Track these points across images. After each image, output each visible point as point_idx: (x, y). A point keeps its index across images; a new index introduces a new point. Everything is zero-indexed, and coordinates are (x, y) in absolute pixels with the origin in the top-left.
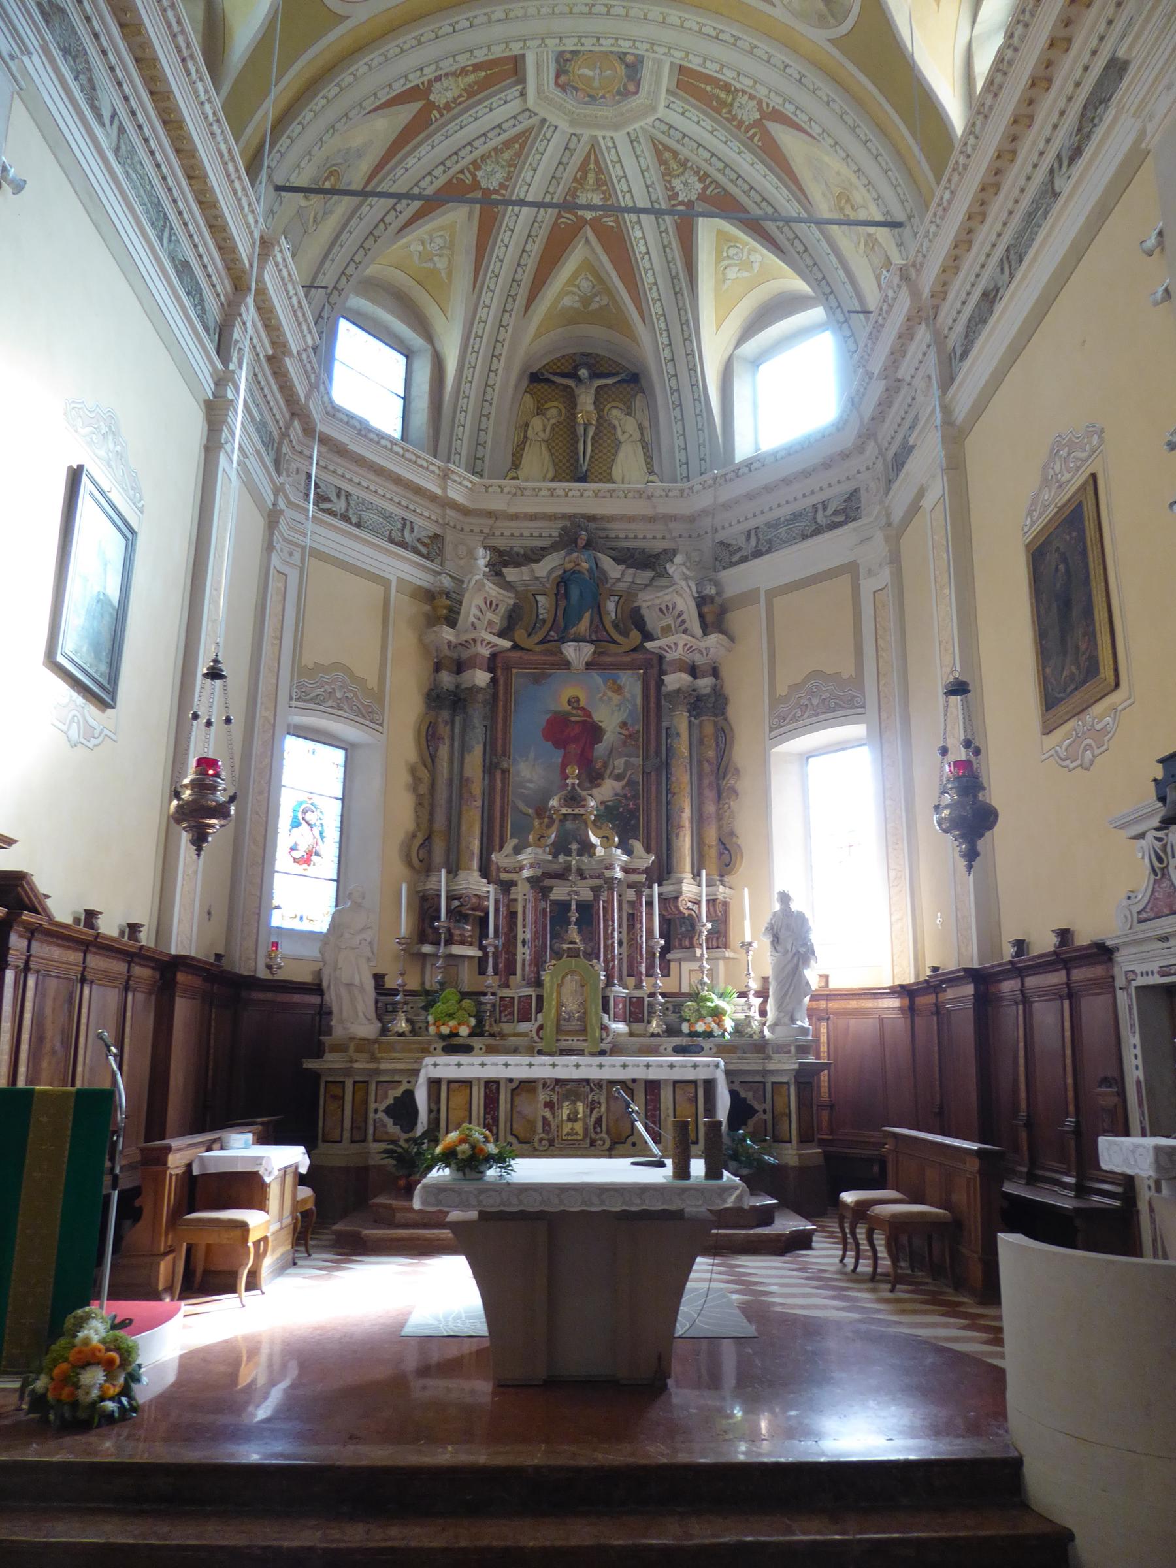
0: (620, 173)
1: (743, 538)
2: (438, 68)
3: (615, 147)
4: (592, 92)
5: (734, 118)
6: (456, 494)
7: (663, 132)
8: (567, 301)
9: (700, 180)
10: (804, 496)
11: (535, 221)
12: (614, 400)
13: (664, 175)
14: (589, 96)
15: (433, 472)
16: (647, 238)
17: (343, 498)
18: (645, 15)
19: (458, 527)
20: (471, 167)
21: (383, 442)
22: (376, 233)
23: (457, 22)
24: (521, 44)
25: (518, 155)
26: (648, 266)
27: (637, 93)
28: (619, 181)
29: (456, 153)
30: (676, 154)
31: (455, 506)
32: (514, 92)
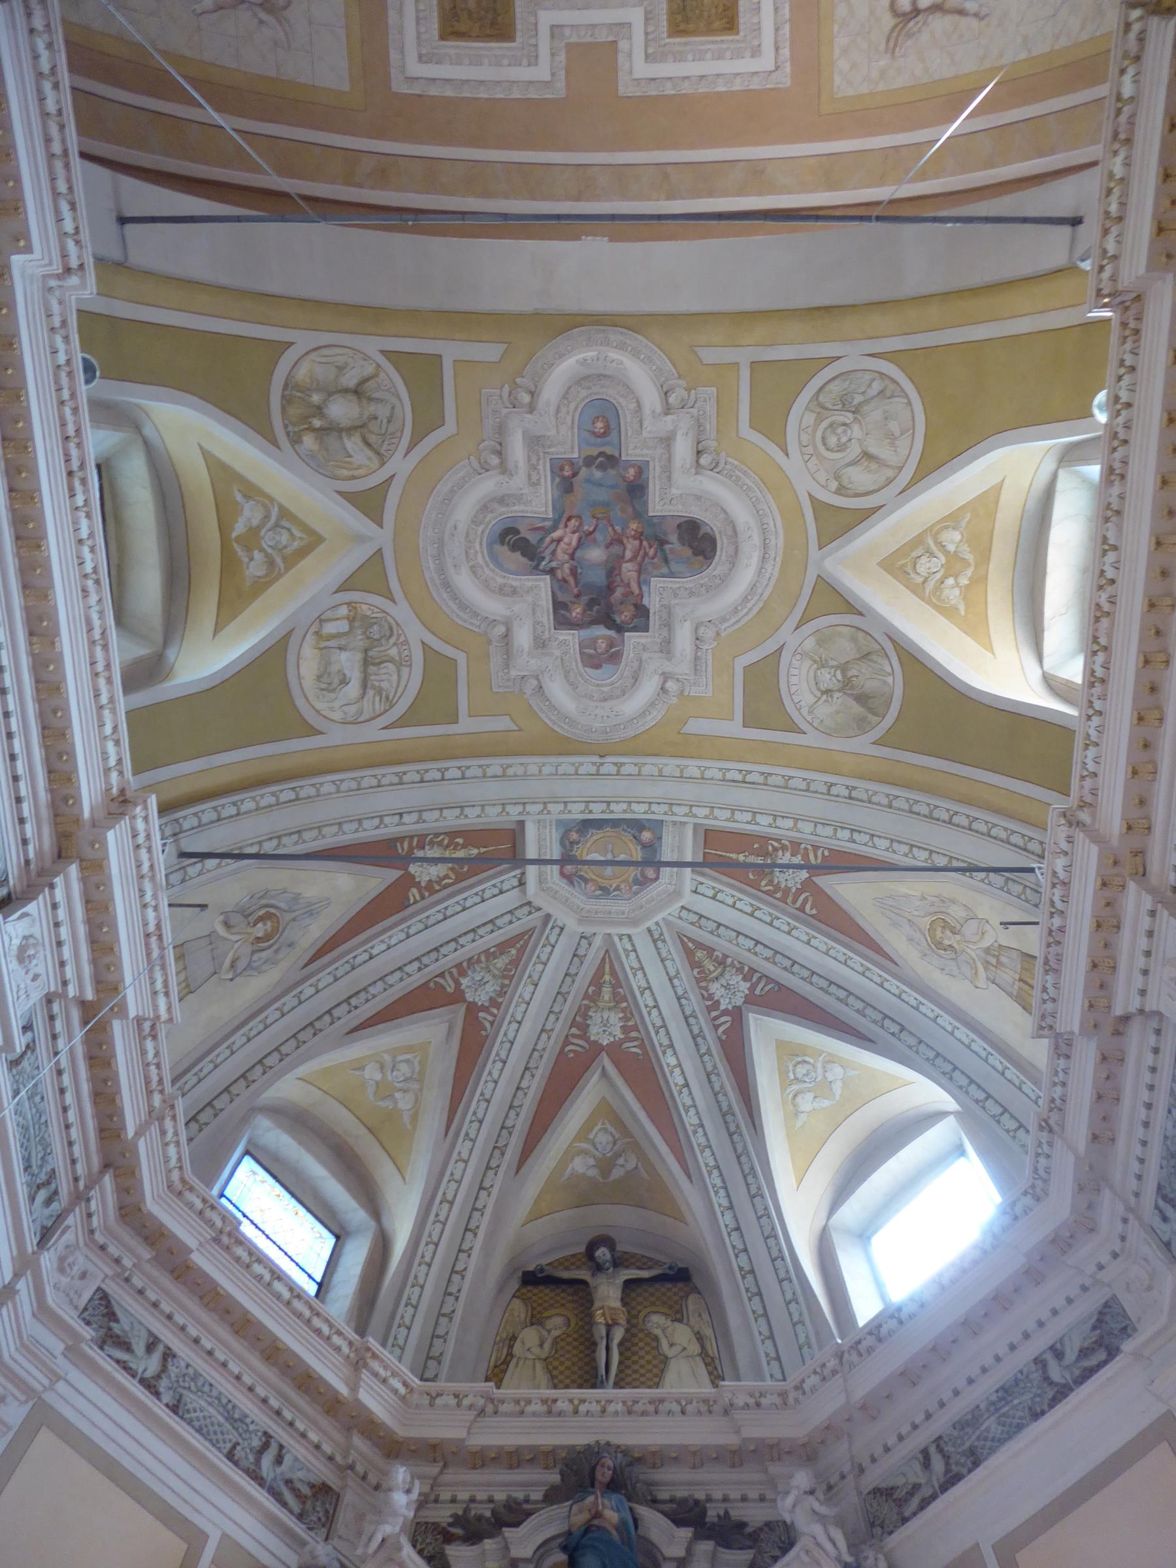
0: (644, 984)
1: (917, 1467)
2: (421, 820)
3: (635, 950)
4: (605, 883)
5: (777, 888)
6: (375, 1401)
7: (692, 924)
8: (579, 1165)
9: (745, 979)
10: (1012, 1347)
11: (534, 1050)
12: (653, 1304)
13: (698, 981)
14: (601, 888)
15: (338, 1349)
16: (683, 1066)
17: (157, 1356)
18: (660, 770)
19: (373, 1479)
20: (454, 971)
21: (258, 1269)
22: (318, 1025)
23: (447, 769)
24: (520, 808)
25: (515, 962)
26: (689, 1102)
27: (657, 879)
28: (642, 994)
29: (436, 949)
30: (710, 950)
31: (369, 1427)
32: (510, 878)
